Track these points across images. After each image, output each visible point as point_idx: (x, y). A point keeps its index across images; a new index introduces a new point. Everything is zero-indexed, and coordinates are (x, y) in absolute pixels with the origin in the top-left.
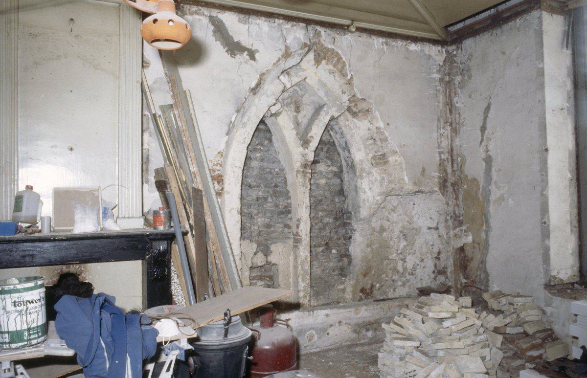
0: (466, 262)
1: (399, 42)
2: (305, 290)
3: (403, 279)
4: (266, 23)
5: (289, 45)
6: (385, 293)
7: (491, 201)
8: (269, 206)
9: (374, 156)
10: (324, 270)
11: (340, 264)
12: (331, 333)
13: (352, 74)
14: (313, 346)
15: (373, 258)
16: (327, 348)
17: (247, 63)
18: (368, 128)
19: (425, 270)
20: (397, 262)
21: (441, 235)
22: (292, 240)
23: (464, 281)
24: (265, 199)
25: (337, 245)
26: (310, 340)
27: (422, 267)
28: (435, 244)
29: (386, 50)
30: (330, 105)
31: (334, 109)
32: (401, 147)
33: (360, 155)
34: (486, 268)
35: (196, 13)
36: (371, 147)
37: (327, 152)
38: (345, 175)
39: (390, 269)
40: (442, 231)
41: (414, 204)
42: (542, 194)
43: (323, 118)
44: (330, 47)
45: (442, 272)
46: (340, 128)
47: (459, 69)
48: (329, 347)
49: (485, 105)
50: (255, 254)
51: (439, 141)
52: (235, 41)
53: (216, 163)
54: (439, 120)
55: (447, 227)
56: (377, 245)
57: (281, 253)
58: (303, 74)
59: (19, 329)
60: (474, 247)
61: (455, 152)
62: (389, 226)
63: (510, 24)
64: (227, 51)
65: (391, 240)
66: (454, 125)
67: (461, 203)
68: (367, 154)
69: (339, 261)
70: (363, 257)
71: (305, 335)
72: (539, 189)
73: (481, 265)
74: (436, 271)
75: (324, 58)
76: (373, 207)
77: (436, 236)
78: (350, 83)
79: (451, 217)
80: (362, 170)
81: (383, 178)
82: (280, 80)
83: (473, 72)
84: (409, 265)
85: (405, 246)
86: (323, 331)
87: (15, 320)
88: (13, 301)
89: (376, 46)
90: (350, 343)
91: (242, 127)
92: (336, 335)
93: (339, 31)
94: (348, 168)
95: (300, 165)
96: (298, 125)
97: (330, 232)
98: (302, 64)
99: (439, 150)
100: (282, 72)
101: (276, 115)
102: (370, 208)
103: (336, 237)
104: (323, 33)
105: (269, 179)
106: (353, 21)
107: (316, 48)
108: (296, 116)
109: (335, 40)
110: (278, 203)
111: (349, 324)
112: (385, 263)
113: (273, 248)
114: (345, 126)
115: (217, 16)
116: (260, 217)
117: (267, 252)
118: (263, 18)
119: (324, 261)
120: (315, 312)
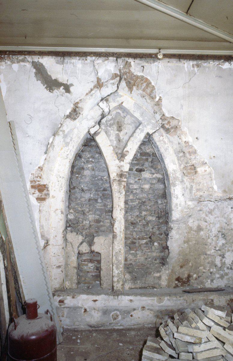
1: (211, 63)
2: (118, 276)
3: (222, 272)
4: (80, 61)
5: (100, 77)
6: (202, 283)
8: (99, 206)
9: (185, 166)
10: (147, 259)
11: (163, 254)
12: (134, 315)
13: (161, 96)
14: (117, 324)
15: (190, 252)
16: (130, 327)
17: (62, 96)
20: (216, 257)
24: (96, 200)
25: (159, 239)
26: (115, 319)
29: (196, 71)
30: (146, 124)
32: (211, 158)
33: (172, 164)
35: (23, 61)
36: (182, 158)
37: (152, 162)
39: (208, 263)
43: (138, 135)
44: (139, 75)
48: (132, 326)
50: (81, 243)
52: (53, 79)
53: (37, 175)
56: (194, 242)
57: (103, 244)
58: (120, 100)
62: (207, 226)
64: (46, 88)
65: (209, 238)
68: (180, 165)
69: (161, 252)
70: (180, 251)
71: (109, 314)
75: (134, 85)
76: (185, 210)
78: (158, 104)
80: (176, 178)
81: (192, 187)
82: (99, 106)
85: (223, 244)
86: (127, 312)
89: (186, 69)
90: (152, 326)
91: (65, 146)
92: (139, 318)
93: (148, 59)
95: (116, 175)
96: (120, 141)
97: (153, 229)
98: (118, 91)
100: (102, 100)
101: (96, 133)
102: (182, 211)
103: (158, 232)
104: (132, 63)
105: (100, 184)
106: (160, 49)
107: (126, 77)
108: (118, 134)
109: (144, 68)
110: (107, 203)
111: (151, 310)
112: (202, 257)
113: (96, 240)
114: (160, 141)
115: (38, 61)
116: (91, 214)
117: (91, 244)
118: (78, 58)
119: (147, 251)
120: (120, 297)
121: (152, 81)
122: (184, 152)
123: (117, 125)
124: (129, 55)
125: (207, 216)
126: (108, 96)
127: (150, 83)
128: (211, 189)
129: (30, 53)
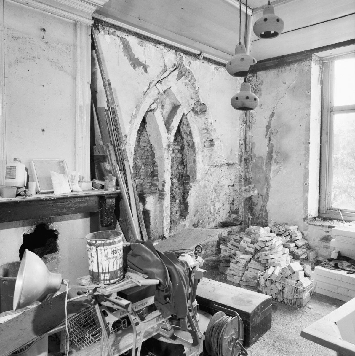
0: (252, 206)
7: (272, 171)
15: (199, 204)
18: (204, 123)
19: (224, 211)
21: (235, 190)
22: (158, 194)
23: (251, 217)
27: (223, 209)
28: (231, 195)
31: (185, 109)
33: (197, 139)
34: (266, 210)
38: (186, 151)
40: (237, 187)
41: (222, 171)
42: (305, 168)
45: (236, 212)
46: (187, 122)
47: (254, 90)
49: (270, 113)
51: (239, 132)
52: (136, 58)
54: (239, 120)
55: (240, 185)
59: (115, 269)
60: (258, 197)
61: (248, 140)
63: (290, 66)
64: (131, 64)
66: (248, 124)
67: (250, 170)
68: (202, 139)
72: (303, 165)
73: (263, 208)
74: (231, 212)
75: (184, 75)
77: (232, 190)
79: (244, 179)
83: (262, 92)
84: (217, 209)
87: (113, 263)
88: (112, 250)
94: (189, 147)
95: (166, 145)
97: (176, 189)
99: (239, 138)
100: (158, 82)
104: (184, 58)
109: (190, 63)
112: (205, 207)
115: (125, 38)
121: (194, 76)
122: (208, 130)
123: (161, 104)
124: (184, 51)
125: (209, 177)
126: (162, 79)
127: (193, 76)
128: (221, 157)
129: (120, 29)
